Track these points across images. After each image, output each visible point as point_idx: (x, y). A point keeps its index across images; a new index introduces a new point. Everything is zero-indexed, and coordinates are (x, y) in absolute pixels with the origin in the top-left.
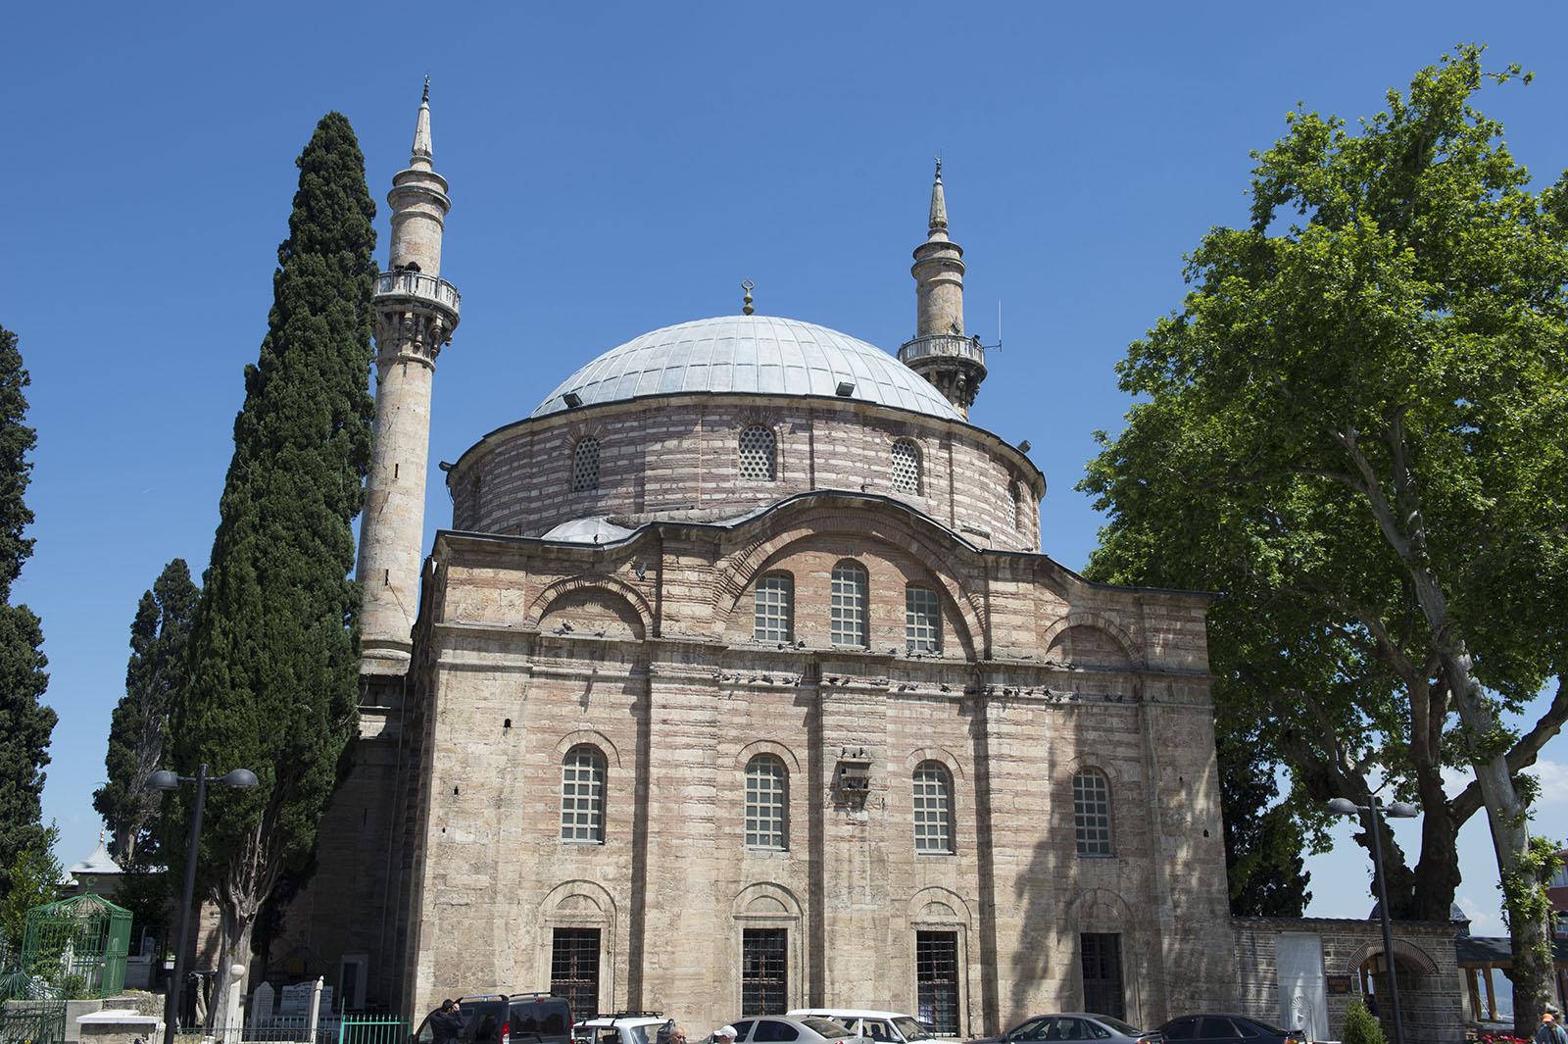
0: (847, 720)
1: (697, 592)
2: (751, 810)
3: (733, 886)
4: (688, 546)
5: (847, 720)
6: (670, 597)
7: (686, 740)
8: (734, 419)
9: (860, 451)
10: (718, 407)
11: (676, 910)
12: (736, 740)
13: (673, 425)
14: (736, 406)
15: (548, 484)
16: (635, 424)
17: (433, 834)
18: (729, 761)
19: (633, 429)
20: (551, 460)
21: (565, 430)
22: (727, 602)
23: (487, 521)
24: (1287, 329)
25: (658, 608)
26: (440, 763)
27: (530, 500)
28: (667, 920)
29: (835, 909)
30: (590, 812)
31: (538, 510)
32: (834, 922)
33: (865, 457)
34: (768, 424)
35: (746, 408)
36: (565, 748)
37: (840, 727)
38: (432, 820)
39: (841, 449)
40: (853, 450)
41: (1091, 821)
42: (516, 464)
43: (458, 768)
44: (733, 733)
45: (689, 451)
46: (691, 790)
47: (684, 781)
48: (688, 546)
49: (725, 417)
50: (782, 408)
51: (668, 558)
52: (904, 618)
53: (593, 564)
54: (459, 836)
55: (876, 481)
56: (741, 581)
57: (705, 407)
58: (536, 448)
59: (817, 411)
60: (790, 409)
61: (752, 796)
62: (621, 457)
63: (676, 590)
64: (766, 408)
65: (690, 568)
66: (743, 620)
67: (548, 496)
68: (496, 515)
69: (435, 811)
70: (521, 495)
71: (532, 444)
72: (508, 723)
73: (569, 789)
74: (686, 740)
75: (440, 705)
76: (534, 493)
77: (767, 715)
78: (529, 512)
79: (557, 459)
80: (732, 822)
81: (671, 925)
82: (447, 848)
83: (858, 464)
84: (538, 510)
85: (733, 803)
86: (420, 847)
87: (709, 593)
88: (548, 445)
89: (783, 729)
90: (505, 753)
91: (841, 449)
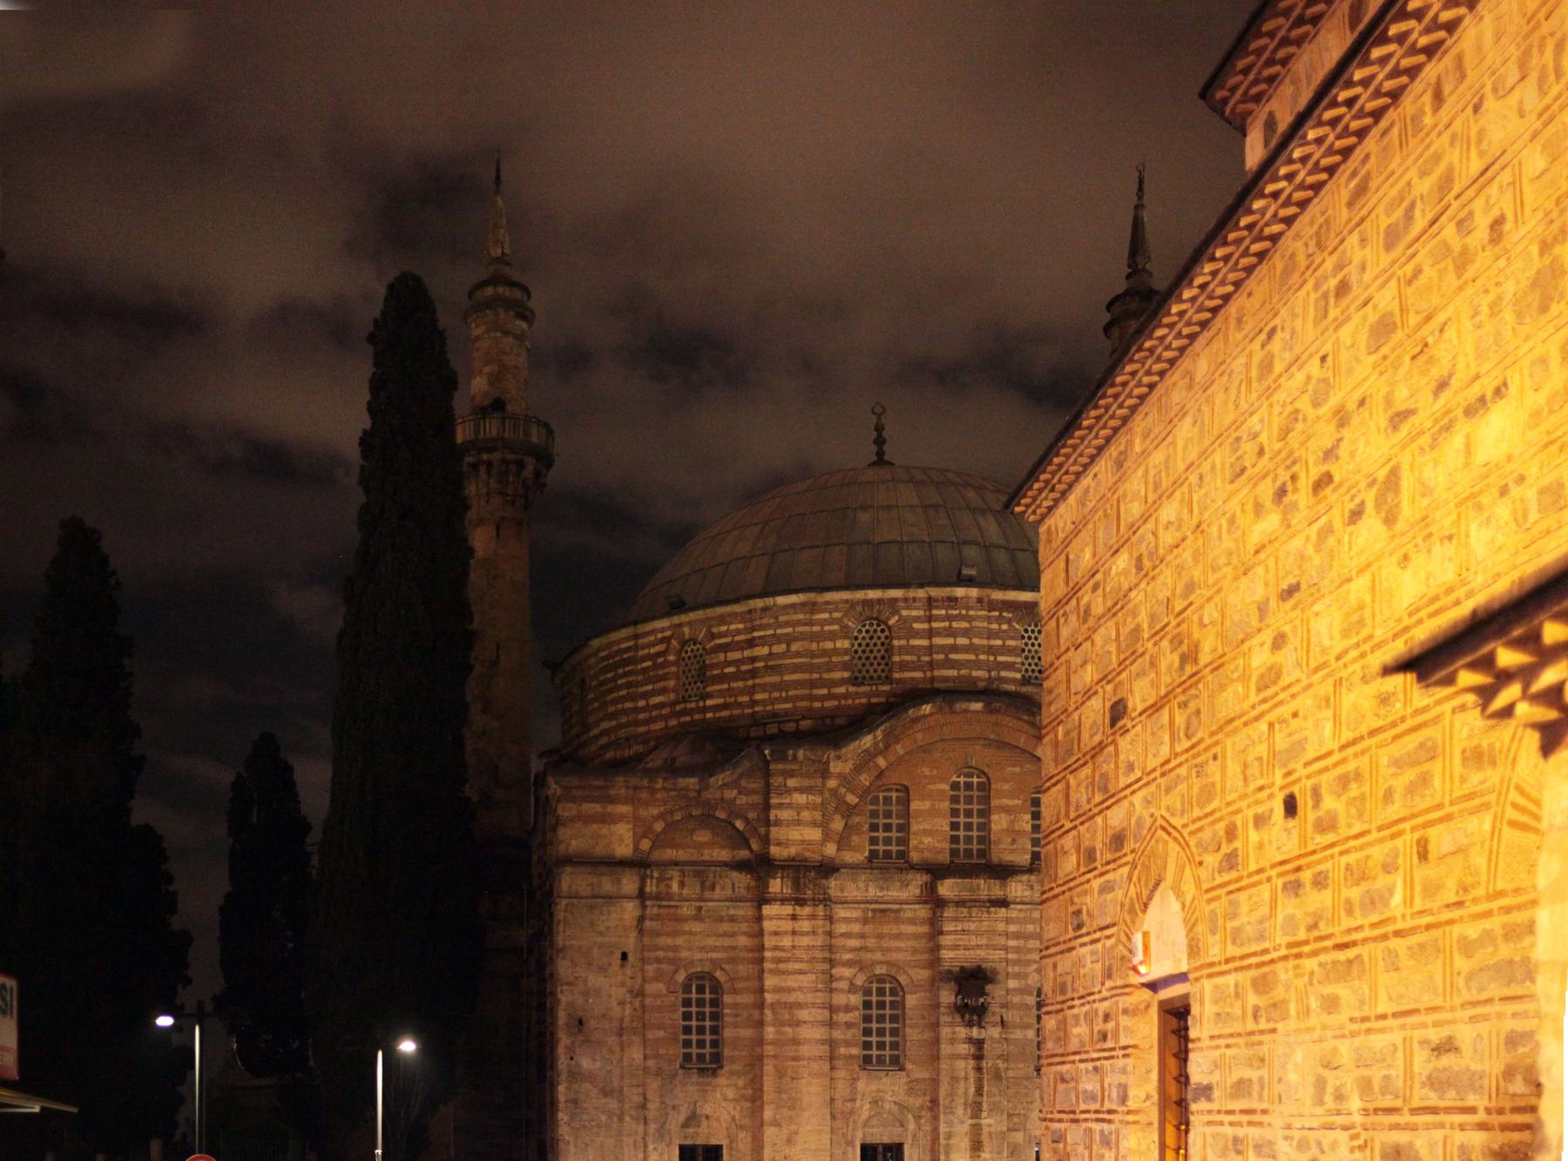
0: (964, 940)
1: (805, 815)
2: (867, 1032)
3: (849, 1105)
4: (795, 767)
5: (964, 940)
6: (778, 823)
7: (797, 966)
8: (845, 615)
9: (985, 642)
10: (827, 603)
11: (793, 1128)
12: (849, 964)
13: (780, 627)
14: (847, 601)
15: (653, 693)
16: (741, 626)
17: (563, 1062)
18: (844, 985)
19: (739, 632)
20: (656, 666)
21: (668, 633)
22: (838, 824)
23: (595, 732)
24: (586, 994)
25: (768, 833)
26: (565, 997)
27: (637, 710)
28: (785, 1137)
29: (950, 1124)
30: (708, 1037)
31: (647, 722)
32: (949, 1136)
33: (991, 647)
34: (883, 618)
35: (858, 602)
36: (681, 977)
37: (956, 947)
38: (561, 1050)
39: (962, 641)
40: (976, 641)
41: (881, 1019)
42: (621, 671)
43: (580, 1001)
44: (847, 956)
45: (798, 654)
46: (804, 1014)
47: (799, 1006)
48: (795, 767)
49: (836, 615)
50: (896, 600)
51: (776, 781)
52: (1028, 827)
53: (699, 792)
54: (586, 1063)
55: (1003, 674)
56: (852, 799)
57: (814, 604)
58: (641, 653)
59: (936, 600)
60: (906, 600)
61: (867, 1019)
62: (730, 663)
63: (785, 815)
64: (879, 601)
65: (801, 790)
66: (855, 839)
67: (656, 707)
68: (605, 725)
69: (564, 1040)
70: (628, 705)
71: (636, 648)
72: (624, 956)
73: (687, 1016)
74: (797, 966)
75: (560, 940)
76: (642, 703)
77: (880, 937)
78: (637, 723)
79: (663, 666)
80: (848, 1044)
81: (790, 1141)
82: (575, 1075)
83: (982, 657)
84: (647, 722)
85: (848, 1025)
86: (552, 1067)
87: (818, 816)
88: (652, 651)
89: (899, 949)
90: (623, 984)
91: (962, 641)
